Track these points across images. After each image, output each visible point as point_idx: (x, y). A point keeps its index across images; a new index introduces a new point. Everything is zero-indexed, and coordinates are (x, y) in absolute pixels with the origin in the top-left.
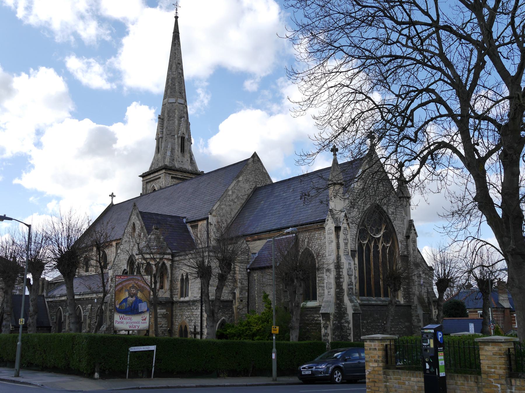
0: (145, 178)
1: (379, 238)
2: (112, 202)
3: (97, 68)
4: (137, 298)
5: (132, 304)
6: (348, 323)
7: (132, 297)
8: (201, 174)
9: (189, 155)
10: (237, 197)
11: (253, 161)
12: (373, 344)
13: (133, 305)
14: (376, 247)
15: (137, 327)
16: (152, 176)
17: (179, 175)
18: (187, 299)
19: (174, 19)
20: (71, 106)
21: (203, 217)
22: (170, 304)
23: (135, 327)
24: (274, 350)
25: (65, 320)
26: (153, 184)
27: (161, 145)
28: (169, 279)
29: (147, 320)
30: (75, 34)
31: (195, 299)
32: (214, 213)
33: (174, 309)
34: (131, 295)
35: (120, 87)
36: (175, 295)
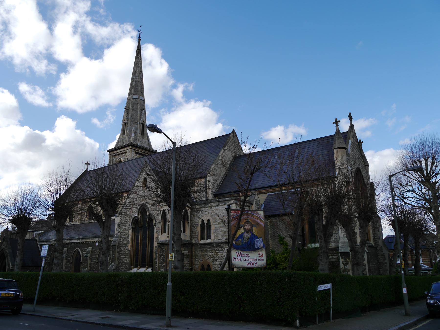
0: (111, 153)
2: (87, 169)
3: (40, 92)
4: (252, 233)
5: (248, 239)
7: (248, 233)
9: (147, 138)
11: (233, 136)
13: (249, 241)
15: (255, 264)
16: (118, 151)
17: (141, 151)
18: (209, 241)
20: (19, 116)
22: (190, 245)
23: (253, 264)
26: (120, 157)
27: (127, 129)
28: (190, 224)
29: (264, 257)
30: (30, 68)
31: (220, 241)
32: (211, 173)
33: (194, 250)
34: (246, 231)
35: (55, 106)
36: (194, 238)
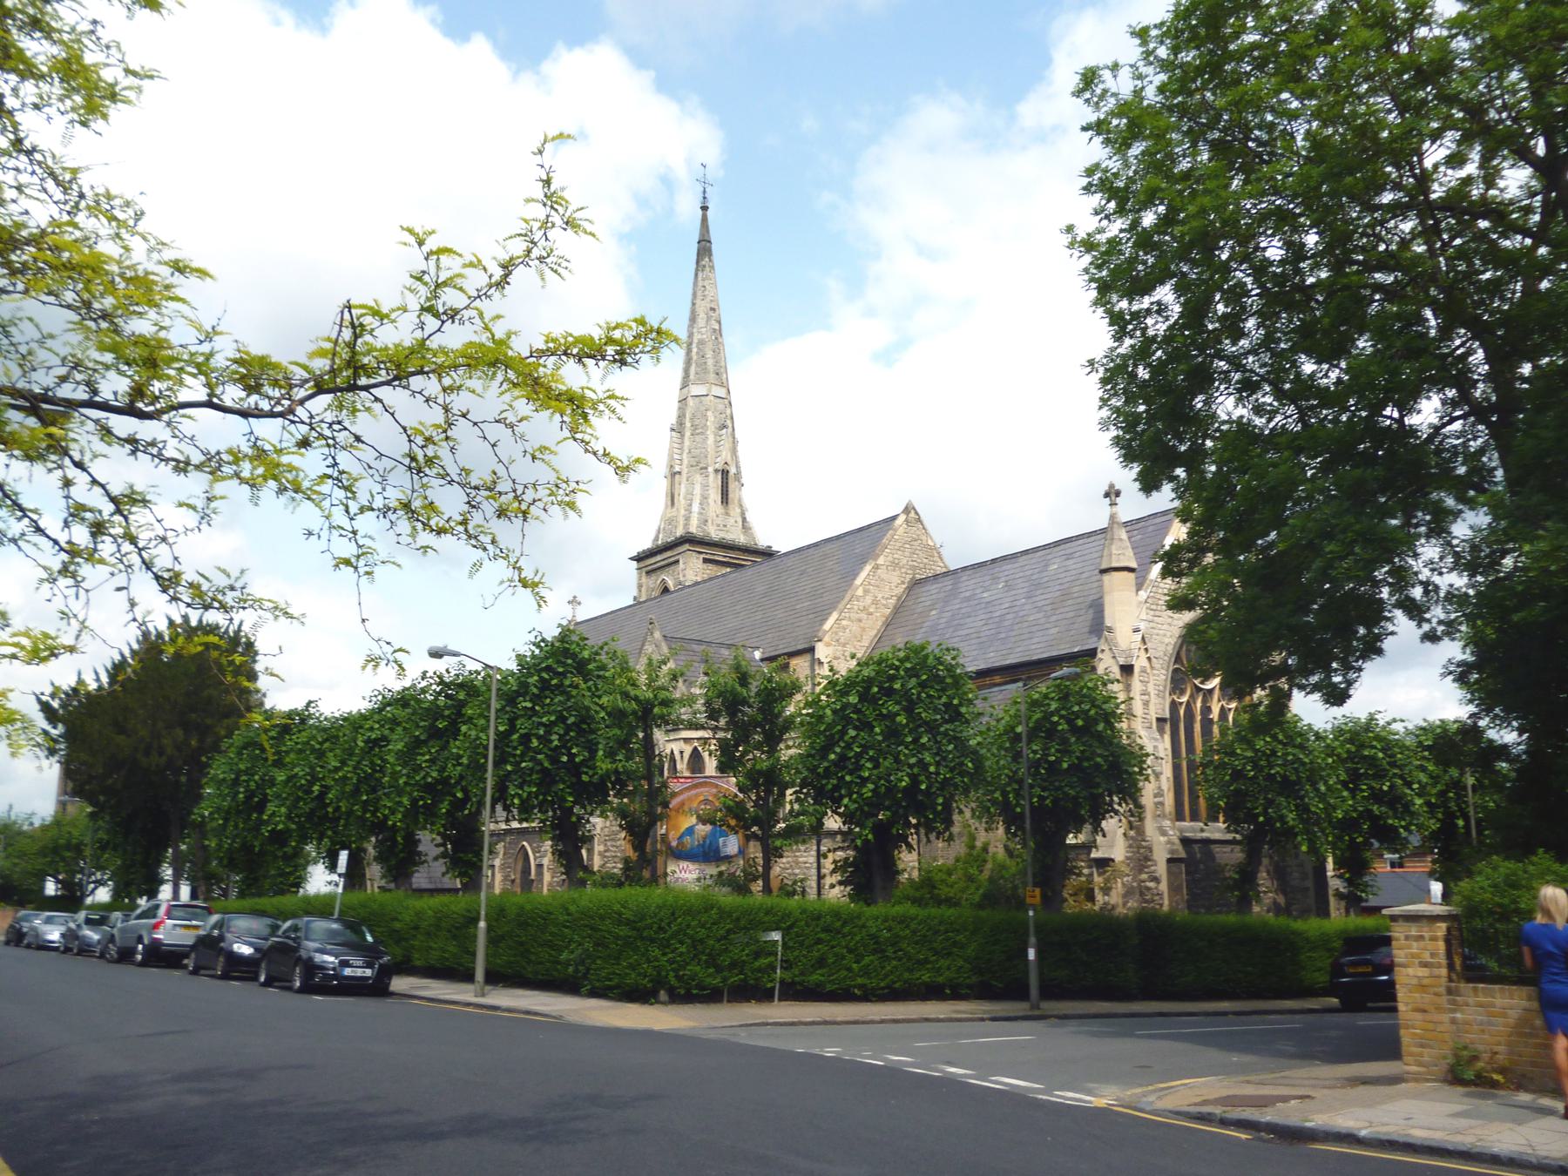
0: (642, 564)
1: (1211, 691)
5: (705, 838)
6: (1156, 880)
8: (768, 554)
10: (875, 602)
14: (1207, 710)
16: (659, 558)
17: (720, 555)
19: (700, 212)
21: (800, 647)
24: (1033, 940)
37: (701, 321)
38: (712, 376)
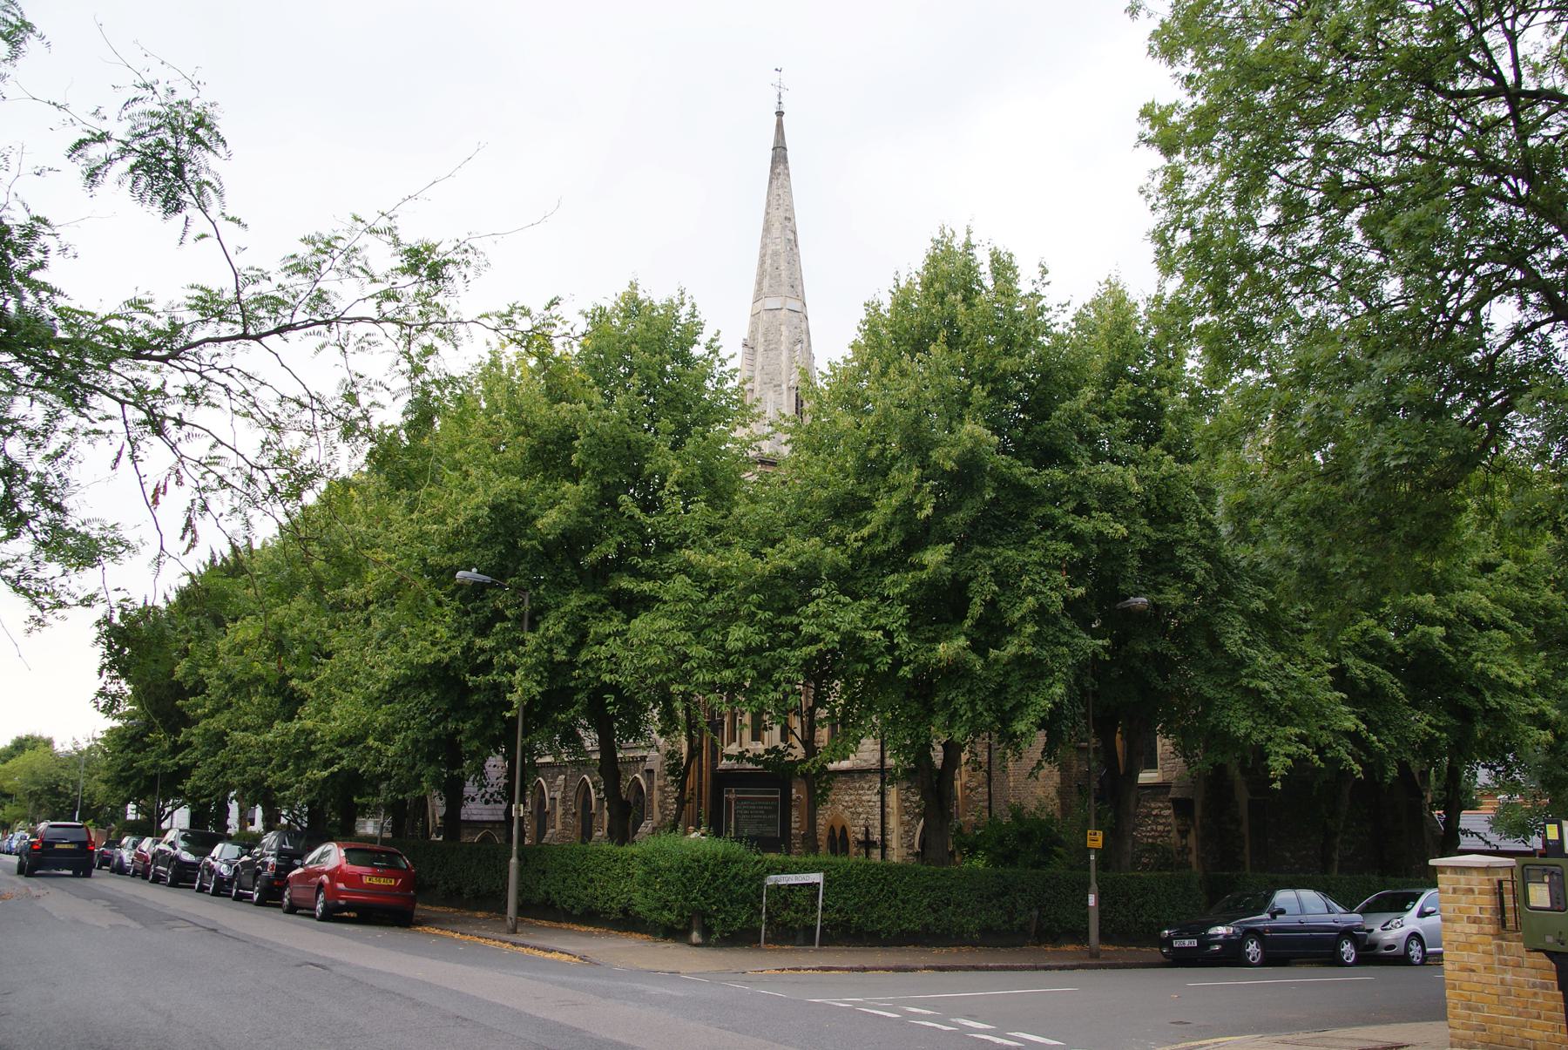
12: (1462, 878)
19: (775, 118)
25: (554, 808)
37: (776, 232)
38: (786, 289)
